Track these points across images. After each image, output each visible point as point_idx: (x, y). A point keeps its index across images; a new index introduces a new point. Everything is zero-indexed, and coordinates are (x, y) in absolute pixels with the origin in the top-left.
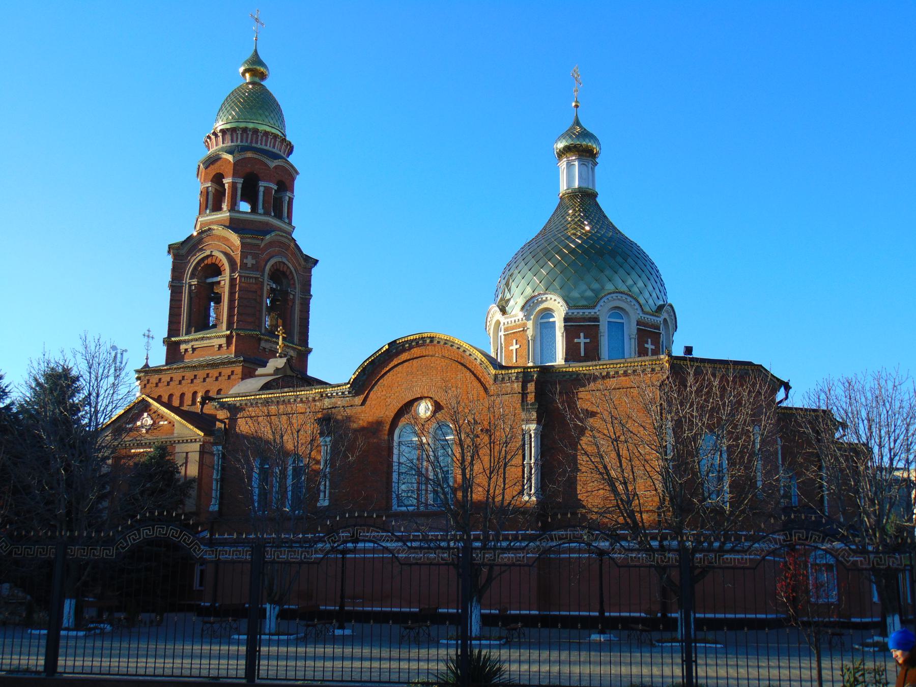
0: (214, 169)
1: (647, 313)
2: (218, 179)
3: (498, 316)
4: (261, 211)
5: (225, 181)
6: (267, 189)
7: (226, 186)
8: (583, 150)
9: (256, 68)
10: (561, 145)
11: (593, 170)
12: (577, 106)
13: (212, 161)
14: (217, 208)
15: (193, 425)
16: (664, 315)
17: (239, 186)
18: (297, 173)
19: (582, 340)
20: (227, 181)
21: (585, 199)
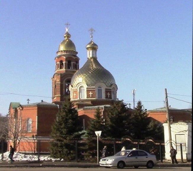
0: (60, 59)
1: (108, 87)
2: (61, 62)
3: (71, 87)
4: (72, 68)
5: (63, 62)
6: (73, 64)
7: (64, 64)
8: (94, 48)
9: (68, 35)
10: (88, 46)
11: (96, 52)
12: (92, 37)
13: (59, 57)
14: (61, 68)
15: (38, 120)
16: (113, 86)
17: (67, 63)
18: (80, 59)
19: (109, 94)
20: (64, 62)
21: (95, 59)
